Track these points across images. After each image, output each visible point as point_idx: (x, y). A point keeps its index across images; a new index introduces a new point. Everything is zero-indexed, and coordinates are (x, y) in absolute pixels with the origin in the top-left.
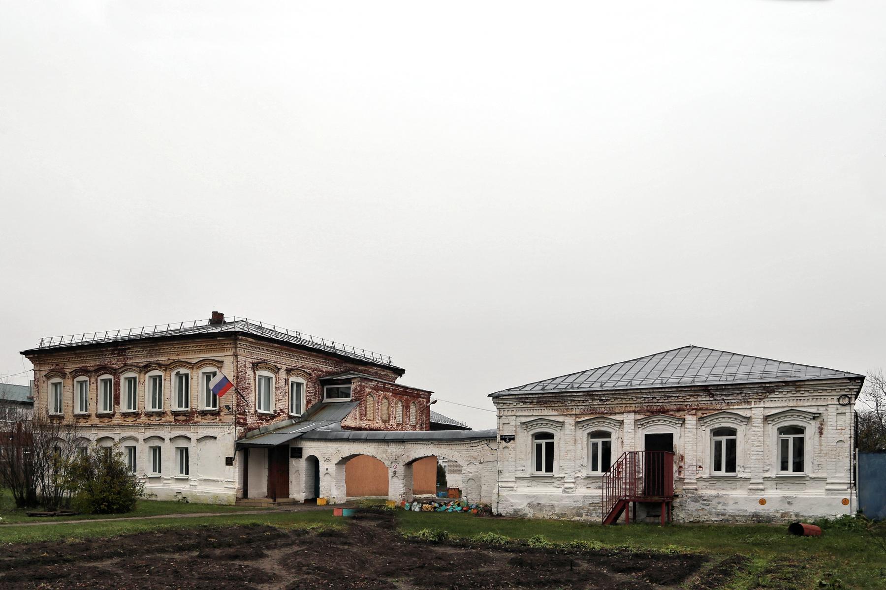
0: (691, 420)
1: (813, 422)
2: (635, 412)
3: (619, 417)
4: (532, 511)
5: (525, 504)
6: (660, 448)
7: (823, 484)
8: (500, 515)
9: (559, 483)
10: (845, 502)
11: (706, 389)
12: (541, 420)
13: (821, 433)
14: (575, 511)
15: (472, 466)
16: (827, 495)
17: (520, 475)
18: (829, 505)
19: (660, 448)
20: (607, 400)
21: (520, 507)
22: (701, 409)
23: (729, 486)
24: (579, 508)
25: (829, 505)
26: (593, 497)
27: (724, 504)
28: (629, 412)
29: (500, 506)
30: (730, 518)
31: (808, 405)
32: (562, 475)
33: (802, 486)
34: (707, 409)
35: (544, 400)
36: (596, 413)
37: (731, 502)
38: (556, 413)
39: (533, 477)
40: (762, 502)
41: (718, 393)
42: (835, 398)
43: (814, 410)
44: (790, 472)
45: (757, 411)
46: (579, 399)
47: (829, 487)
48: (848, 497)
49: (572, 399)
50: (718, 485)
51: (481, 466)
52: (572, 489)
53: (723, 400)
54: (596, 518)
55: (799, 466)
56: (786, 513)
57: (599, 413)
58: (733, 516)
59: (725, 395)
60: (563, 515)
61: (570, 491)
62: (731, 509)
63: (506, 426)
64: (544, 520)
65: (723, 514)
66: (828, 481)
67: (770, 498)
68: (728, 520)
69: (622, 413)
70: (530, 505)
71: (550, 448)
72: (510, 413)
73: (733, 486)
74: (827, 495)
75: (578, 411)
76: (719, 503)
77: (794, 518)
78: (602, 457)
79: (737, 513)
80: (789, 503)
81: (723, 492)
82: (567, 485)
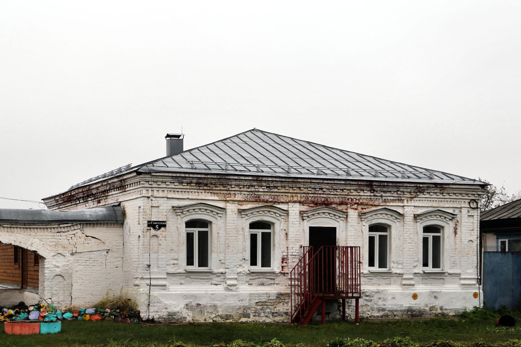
0: (353, 214)
1: (450, 222)
2: (300, 202)
3: (284, 207)
4: (191, 314)
5: (182, 305)
6: (322, 240)
7: (457, 279)
8: (152, 321)
9: (218, 279)
10: (475, 295)
11: (370, 185)
12: (204, 205)
13: (456, 233)
14: (240, 312)
15: (60, 259)
16: (463, 289)
17: (172, 270)
18: (464, 298)
19: (322, 240)
20: (276, 187)
21: (176, 310)
22: (362, 204)
23: (384, 281)
24: (245, 308)
25: (464, 298)
26: (259, 295)
27: (384, 300)
28: (295, 202)
29: (152, 309)
30: (389, 313)
31: (447, 204)
32: (222, 270)
33: (442, 281)
34: (367, 205)
35: (205, 182)
36: (260, 201)
37: (390, 298)
38: (216, 198)
39: (189, 273)
40: (415, 296)
41: (379, 189)
42: (467, 201)
43: (451, 211)
44: (195, 267)
45: (410, 208)
46: (246, 183)
47: (463, 282)
48: (477, 291)
49: (238, 183)
50: (375, 280)
51: (72, 258)
52: (237, 288)
53: (382, 196)
54: (264, 319)
55: (204, 262)
56: (433, 307)
57: (263, 201)
58: (392, 311)
59: (384, 192)
60: (228, 317)
61: (233, 288)
62: (390, 305)
63: (154, 210)
64: (206, 325)
65: (383, 310)
66: (462, 277)
67: (421, 293)
68: (387, 316)
69: (287, 203)
70: (188, 306)
71: (204, 238)
72: (161, 194)
73: (387, 281)
74: (403, 289)
75: (239, 197)
76: (380, 299)
77: (439, 311)
78: (261, 248)
79: (395, 308)
80: (435, 297)
81: (381, 288)
82: (229, 282)
